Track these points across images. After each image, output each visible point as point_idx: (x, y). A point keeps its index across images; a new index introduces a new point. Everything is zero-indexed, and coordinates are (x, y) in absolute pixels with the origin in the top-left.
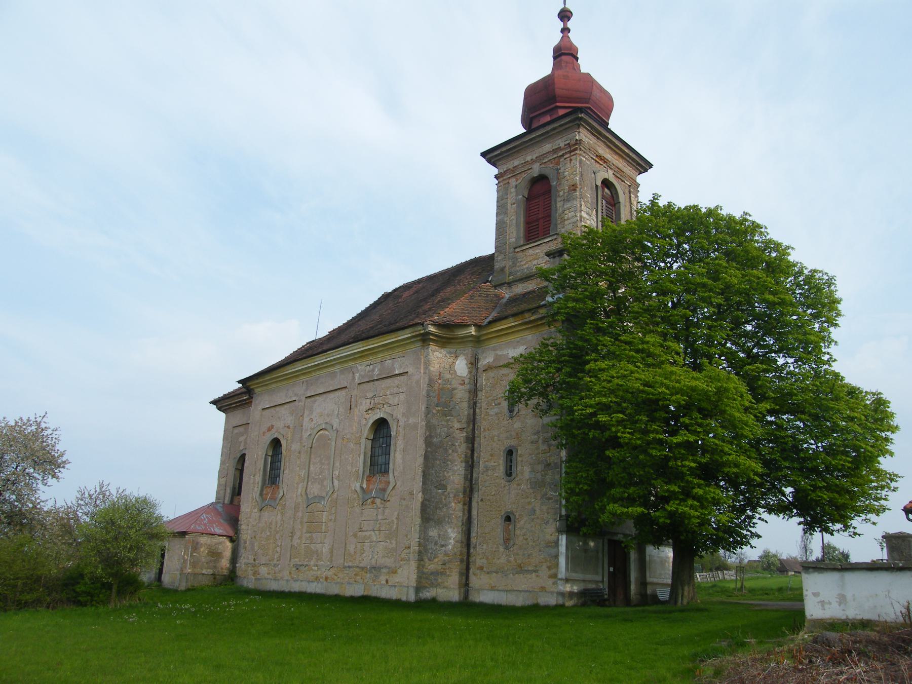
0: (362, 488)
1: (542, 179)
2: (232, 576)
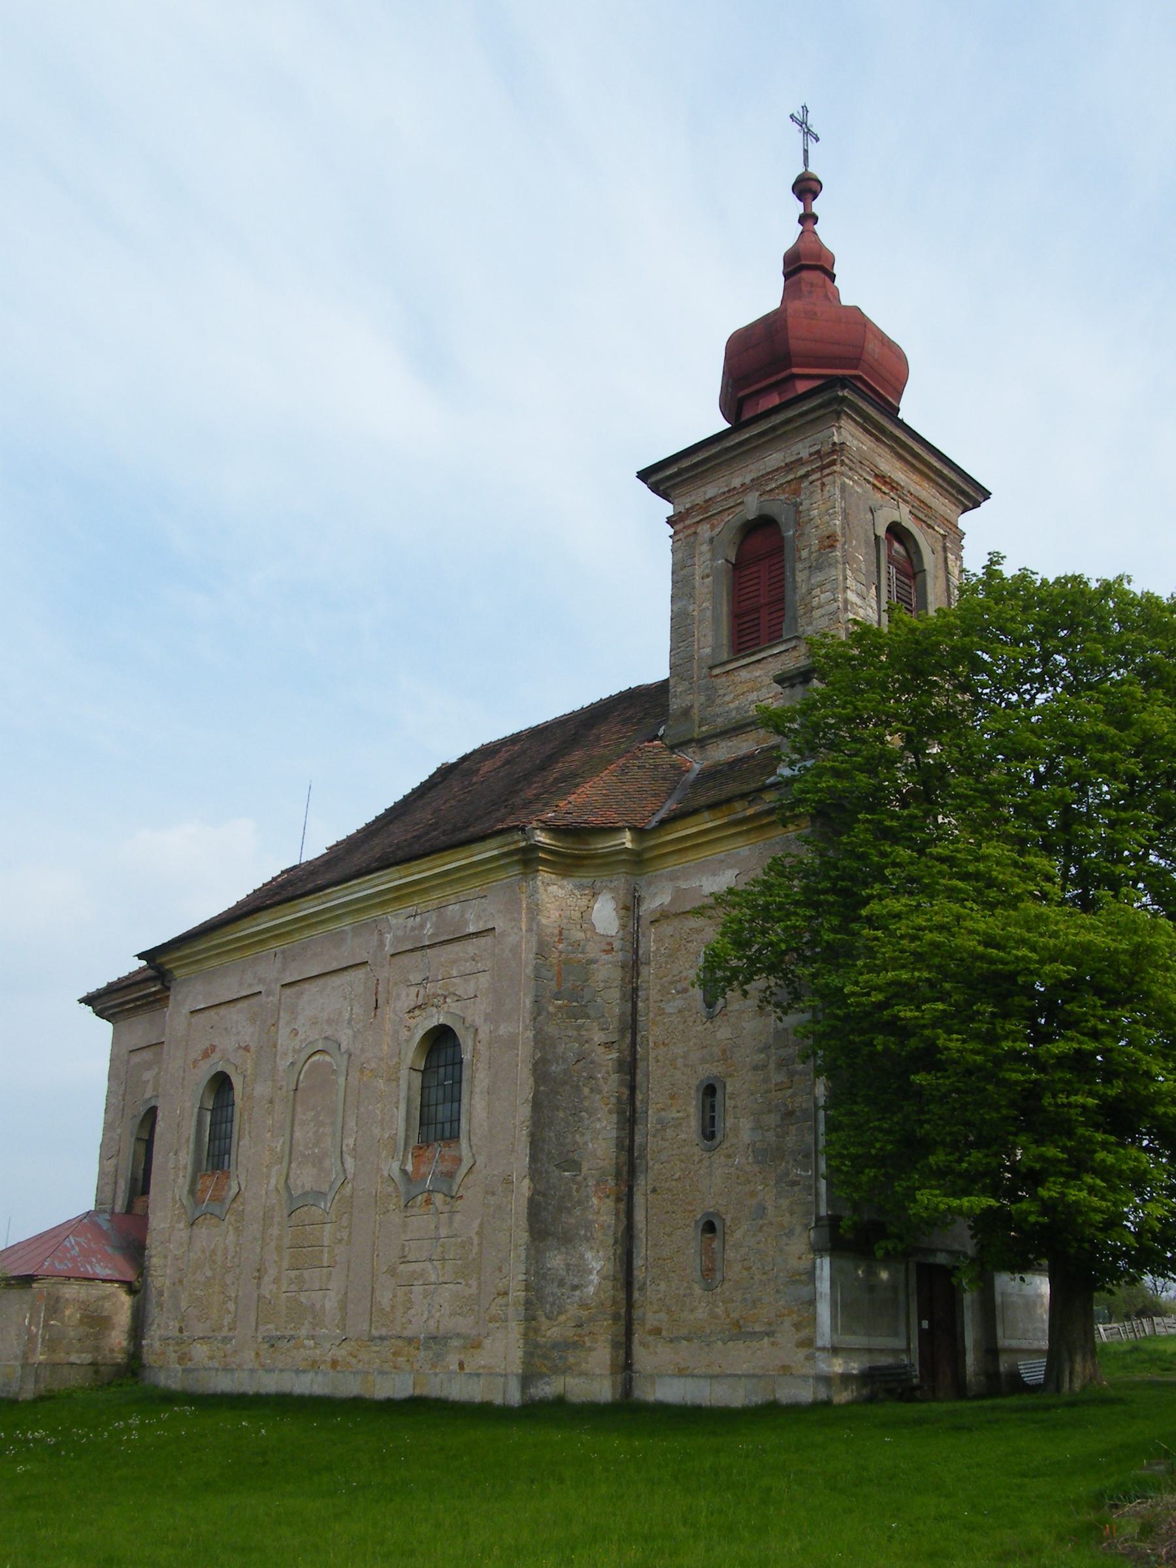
0: (404, 1172)
2: (134, 1364)
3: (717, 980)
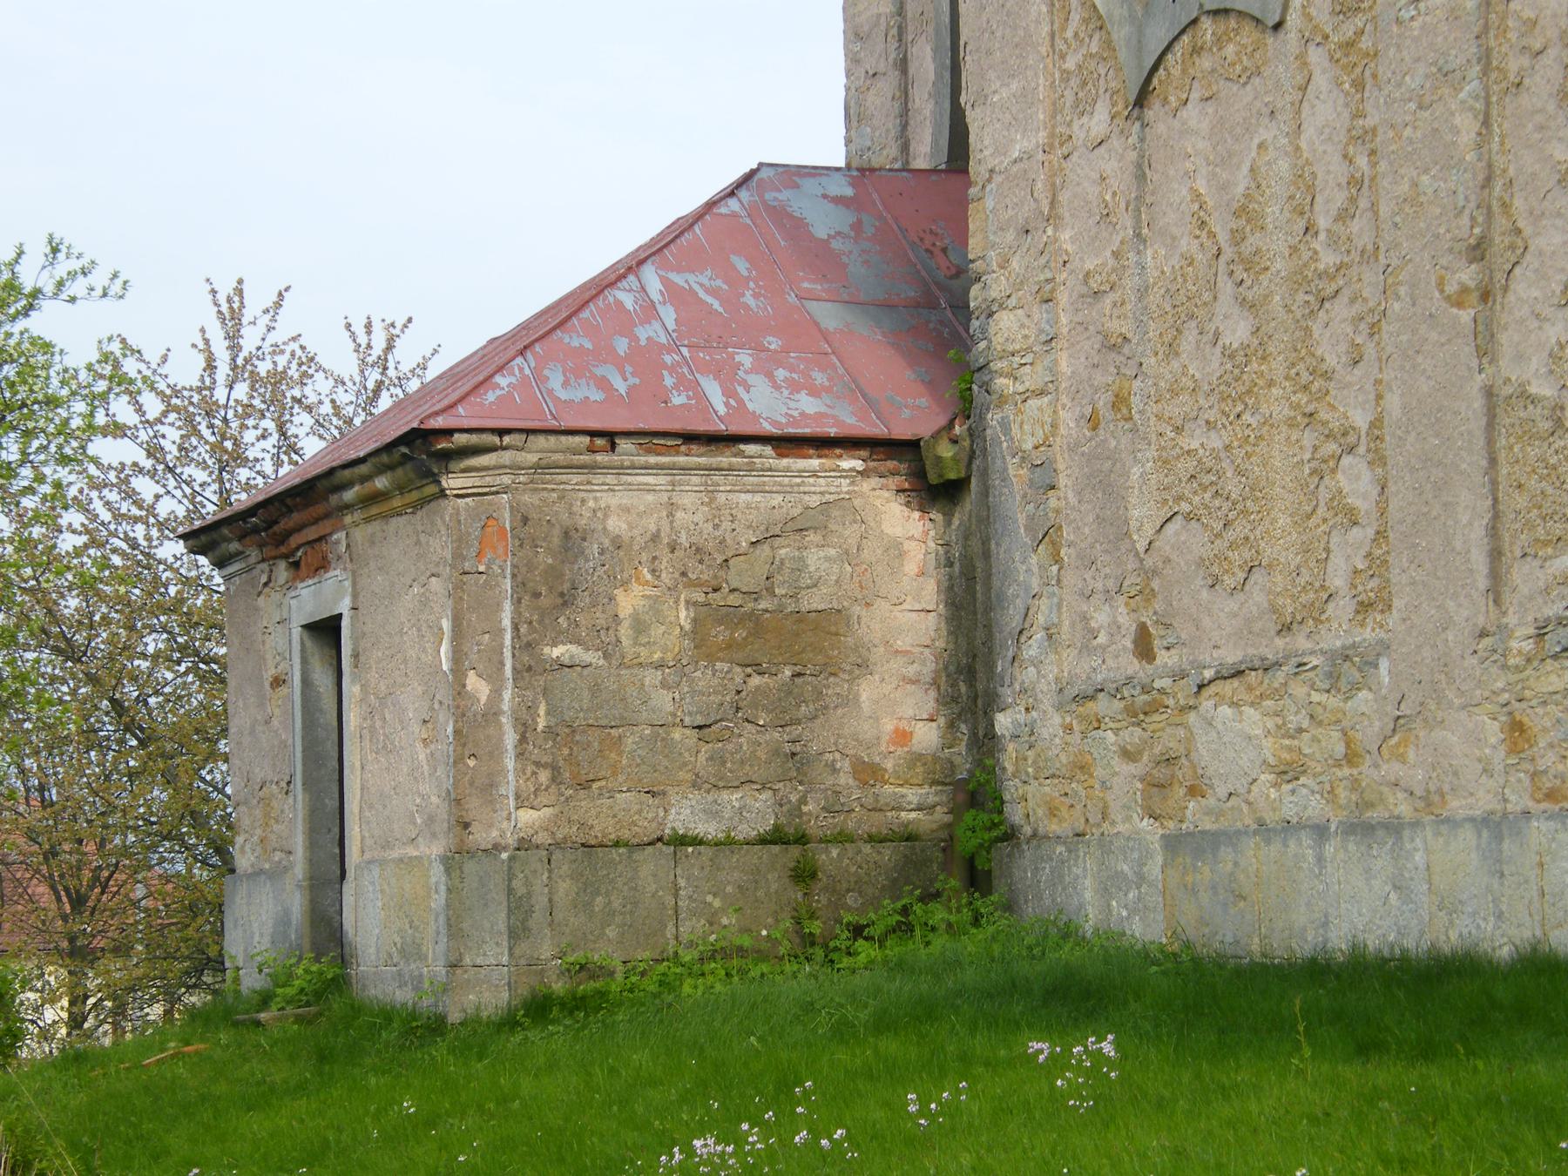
2: (971, 844)
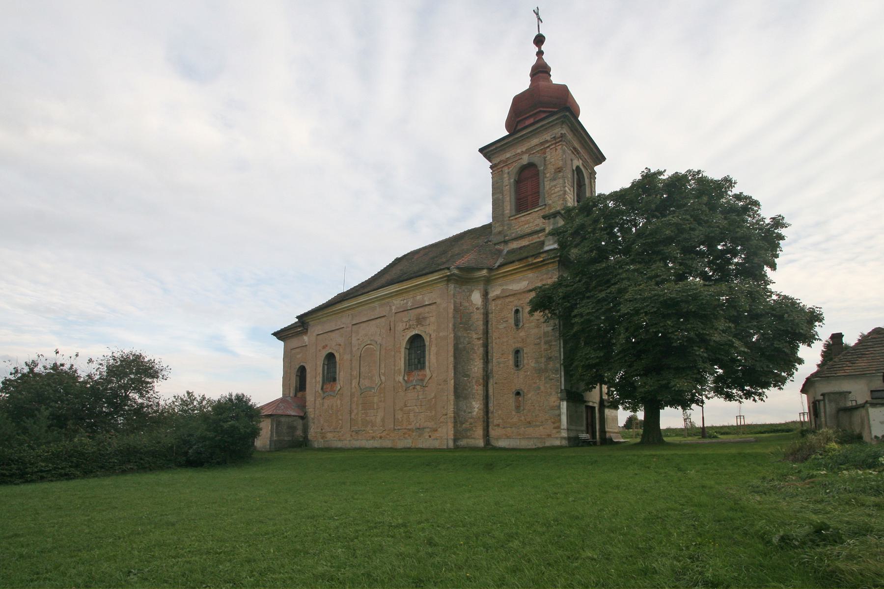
1: (531, 165)
3: (531, 312)
